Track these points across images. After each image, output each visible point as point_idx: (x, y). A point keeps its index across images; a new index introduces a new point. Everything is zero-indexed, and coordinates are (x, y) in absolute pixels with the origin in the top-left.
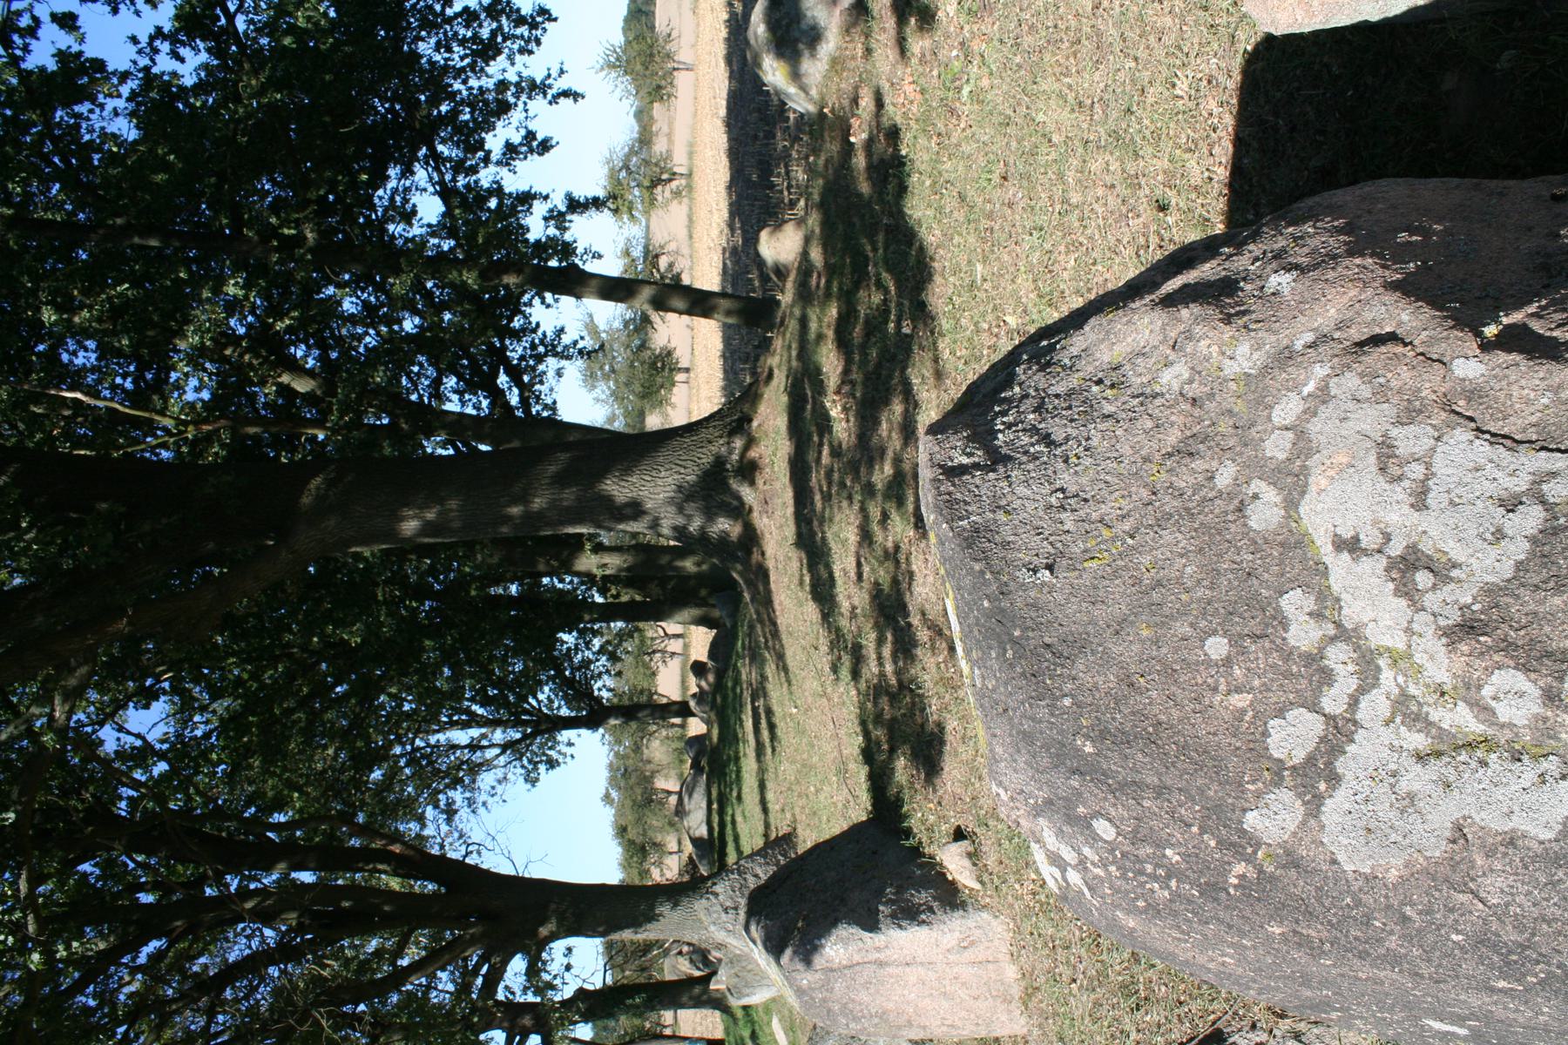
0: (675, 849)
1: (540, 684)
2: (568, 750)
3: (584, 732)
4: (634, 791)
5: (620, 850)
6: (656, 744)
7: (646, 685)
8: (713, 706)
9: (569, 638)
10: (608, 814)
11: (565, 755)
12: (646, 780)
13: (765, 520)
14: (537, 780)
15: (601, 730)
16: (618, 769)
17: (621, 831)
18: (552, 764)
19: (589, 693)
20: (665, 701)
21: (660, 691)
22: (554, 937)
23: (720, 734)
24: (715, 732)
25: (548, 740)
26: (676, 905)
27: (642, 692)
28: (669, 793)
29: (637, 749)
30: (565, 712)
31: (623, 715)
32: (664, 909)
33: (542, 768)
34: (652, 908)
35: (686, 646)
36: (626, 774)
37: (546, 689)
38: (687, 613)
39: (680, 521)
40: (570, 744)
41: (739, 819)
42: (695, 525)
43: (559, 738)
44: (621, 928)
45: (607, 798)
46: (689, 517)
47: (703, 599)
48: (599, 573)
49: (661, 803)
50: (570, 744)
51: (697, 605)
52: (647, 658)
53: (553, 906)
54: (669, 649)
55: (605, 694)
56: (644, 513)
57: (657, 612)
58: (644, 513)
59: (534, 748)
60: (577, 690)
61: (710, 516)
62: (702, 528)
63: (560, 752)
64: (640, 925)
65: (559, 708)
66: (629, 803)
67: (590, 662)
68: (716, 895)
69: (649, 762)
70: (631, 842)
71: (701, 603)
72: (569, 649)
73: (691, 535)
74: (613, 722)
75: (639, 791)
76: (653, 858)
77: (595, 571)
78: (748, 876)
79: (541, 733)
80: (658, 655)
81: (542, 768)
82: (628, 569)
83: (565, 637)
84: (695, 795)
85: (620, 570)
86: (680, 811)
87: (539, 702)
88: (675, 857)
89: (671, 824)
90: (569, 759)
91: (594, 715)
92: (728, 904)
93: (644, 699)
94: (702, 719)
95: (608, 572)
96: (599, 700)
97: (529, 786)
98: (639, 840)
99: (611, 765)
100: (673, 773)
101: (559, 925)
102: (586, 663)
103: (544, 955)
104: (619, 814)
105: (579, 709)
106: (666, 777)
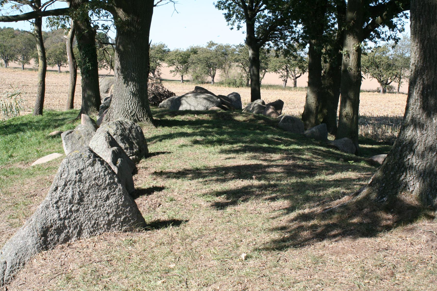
0: (184, 79)
1: (273, 12)
2: (235, 27)
3: (245, 36)
4: (212, 60)
5: (185, 50)
6: (239, 70)
7: (270, 66)
8: (257, 118)
9: (299, 28)
10: (203, 44)
11: (233, 24)
12: (221, 65)
13: (425, 237)
14: (220, 8)
15: (244, 44)
16: (226, 51)
17: (195, 51)
18: (228, 17)
19: (267, 39)
20: (261, 76)
21: (267, 74)
22: (116, 17)
23: (238, 122)
24: (240, 118)
25: (242, 15)
26: (134, 95)
27: (267, 64)
28: (213, 77)
29: (237, 61)
30: (257, 25)
31: (254, 58)
32: (132, 87)
33: (226, 11)
34: (133, 80)
35: (290, 88)
36: (225, 54)
37: (270, 15)
38: (312, 100)
39: (420, 148)
40: (239, 27)
41: (182, 141)
42: (413, 160)
43: (243, 21)
44: (121, 60)
45: (212, 44)
46: (422, 156)
47: (321, 111)
48: (344, 51)
49: (208, 73)
50: (239, 27)
51: (317, 107)
52: (284, 67)
53: (135, 18)
54: (289, 80)
55: (267, 47)
56: (429, 115)
57: (313, 83)
58: (429, 115)
59: (237, 7)
60: (269, 31)
61: (425, 175)
62: (411, 167)
63: (234, 22)
64: (122, 72)
65: (259, 22)
66: (209, 55)
67: (285, 40)
68: (93, 164)
69: (230, 67)
70: (189, 56)
71: (319, 110)
72: (292, 28)
73: (402, 157)
74: (251, 52)
75: (215, 61)
76: (180, 67)
77: (345, 49)
78: (107, 191)
79: (246, 12)
80: (286, 73)
81: (226, 11)
82: (346, 71)
83: (300, 26)
84: (205, 101)
85: (346, 66)
86: (199, 91)
87: (263, 10)
88: (180, 78)
89: (197, 77)
90: (230, 26)
91: (254, 41)
92: (84, 174)
93: (262, 65)
94: (250, 105)
95: (344, 58)
96: (263, 43)
97: (216, 3)
98: (190, 60)
99: (229, 47)
100: (224, 79)
101: (127, 23)
102: (284, 38)
103: (103, 12)
104: (204, 51)
105: (258, 33)
106: (221, 76)
